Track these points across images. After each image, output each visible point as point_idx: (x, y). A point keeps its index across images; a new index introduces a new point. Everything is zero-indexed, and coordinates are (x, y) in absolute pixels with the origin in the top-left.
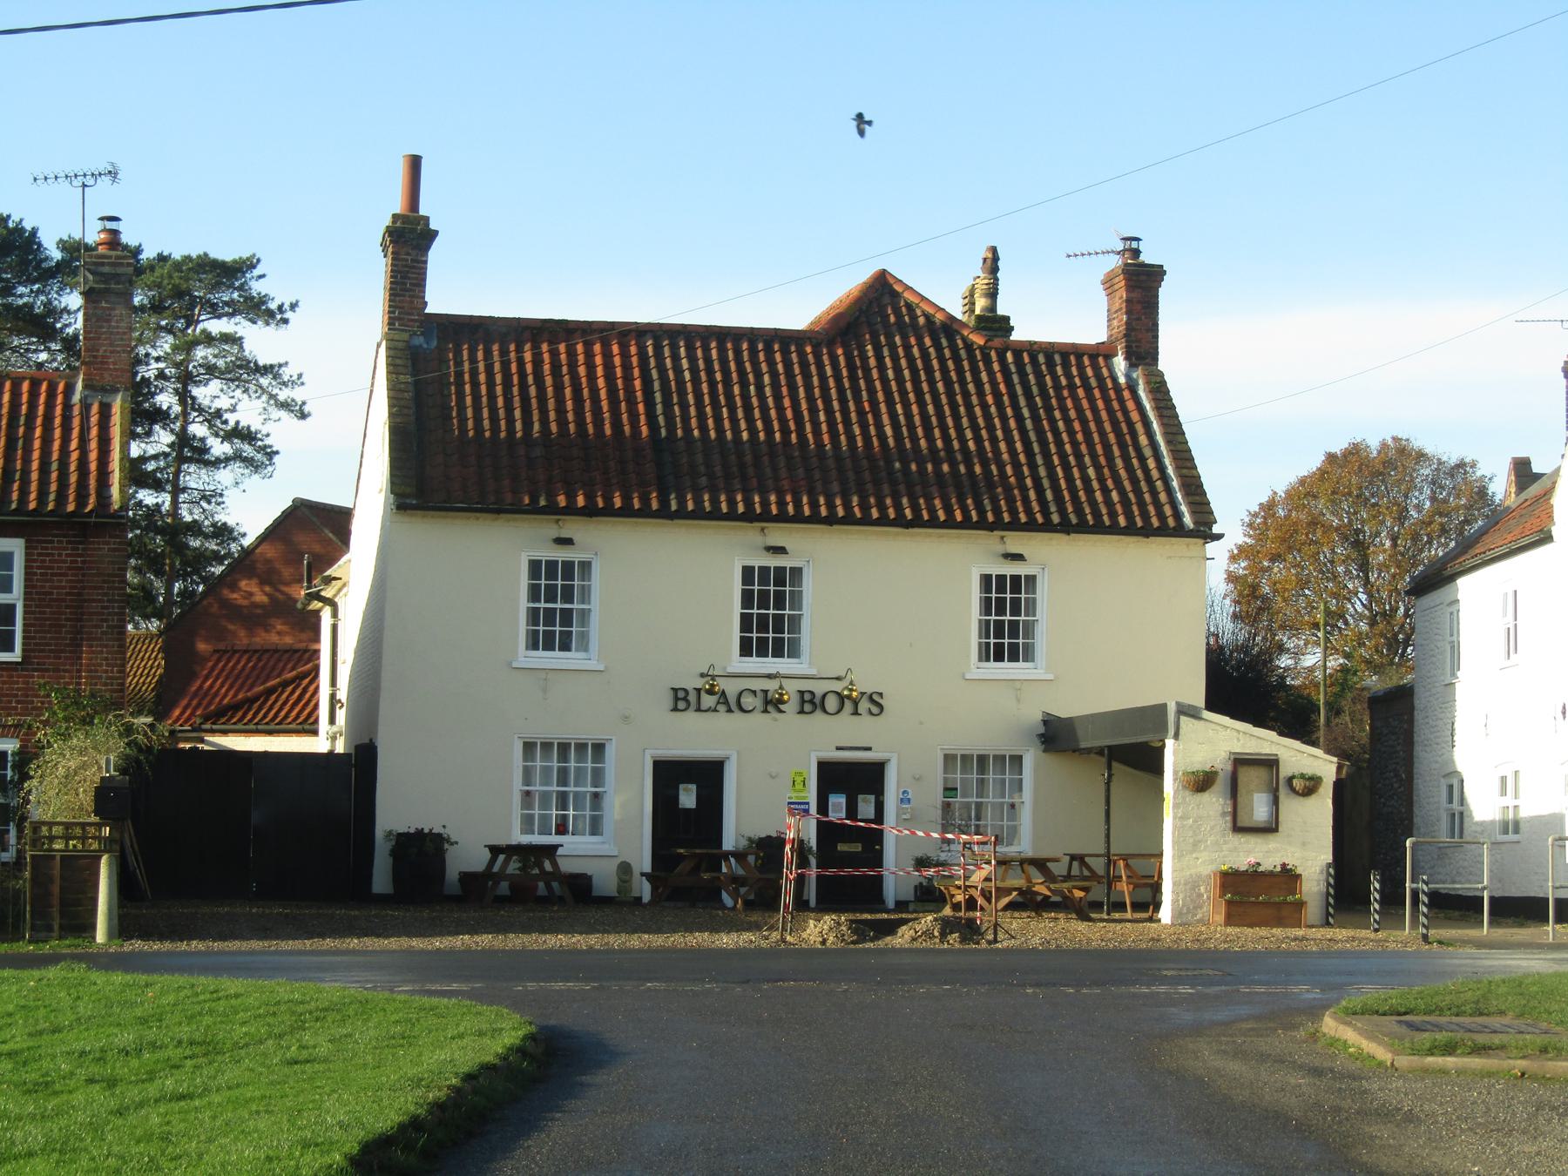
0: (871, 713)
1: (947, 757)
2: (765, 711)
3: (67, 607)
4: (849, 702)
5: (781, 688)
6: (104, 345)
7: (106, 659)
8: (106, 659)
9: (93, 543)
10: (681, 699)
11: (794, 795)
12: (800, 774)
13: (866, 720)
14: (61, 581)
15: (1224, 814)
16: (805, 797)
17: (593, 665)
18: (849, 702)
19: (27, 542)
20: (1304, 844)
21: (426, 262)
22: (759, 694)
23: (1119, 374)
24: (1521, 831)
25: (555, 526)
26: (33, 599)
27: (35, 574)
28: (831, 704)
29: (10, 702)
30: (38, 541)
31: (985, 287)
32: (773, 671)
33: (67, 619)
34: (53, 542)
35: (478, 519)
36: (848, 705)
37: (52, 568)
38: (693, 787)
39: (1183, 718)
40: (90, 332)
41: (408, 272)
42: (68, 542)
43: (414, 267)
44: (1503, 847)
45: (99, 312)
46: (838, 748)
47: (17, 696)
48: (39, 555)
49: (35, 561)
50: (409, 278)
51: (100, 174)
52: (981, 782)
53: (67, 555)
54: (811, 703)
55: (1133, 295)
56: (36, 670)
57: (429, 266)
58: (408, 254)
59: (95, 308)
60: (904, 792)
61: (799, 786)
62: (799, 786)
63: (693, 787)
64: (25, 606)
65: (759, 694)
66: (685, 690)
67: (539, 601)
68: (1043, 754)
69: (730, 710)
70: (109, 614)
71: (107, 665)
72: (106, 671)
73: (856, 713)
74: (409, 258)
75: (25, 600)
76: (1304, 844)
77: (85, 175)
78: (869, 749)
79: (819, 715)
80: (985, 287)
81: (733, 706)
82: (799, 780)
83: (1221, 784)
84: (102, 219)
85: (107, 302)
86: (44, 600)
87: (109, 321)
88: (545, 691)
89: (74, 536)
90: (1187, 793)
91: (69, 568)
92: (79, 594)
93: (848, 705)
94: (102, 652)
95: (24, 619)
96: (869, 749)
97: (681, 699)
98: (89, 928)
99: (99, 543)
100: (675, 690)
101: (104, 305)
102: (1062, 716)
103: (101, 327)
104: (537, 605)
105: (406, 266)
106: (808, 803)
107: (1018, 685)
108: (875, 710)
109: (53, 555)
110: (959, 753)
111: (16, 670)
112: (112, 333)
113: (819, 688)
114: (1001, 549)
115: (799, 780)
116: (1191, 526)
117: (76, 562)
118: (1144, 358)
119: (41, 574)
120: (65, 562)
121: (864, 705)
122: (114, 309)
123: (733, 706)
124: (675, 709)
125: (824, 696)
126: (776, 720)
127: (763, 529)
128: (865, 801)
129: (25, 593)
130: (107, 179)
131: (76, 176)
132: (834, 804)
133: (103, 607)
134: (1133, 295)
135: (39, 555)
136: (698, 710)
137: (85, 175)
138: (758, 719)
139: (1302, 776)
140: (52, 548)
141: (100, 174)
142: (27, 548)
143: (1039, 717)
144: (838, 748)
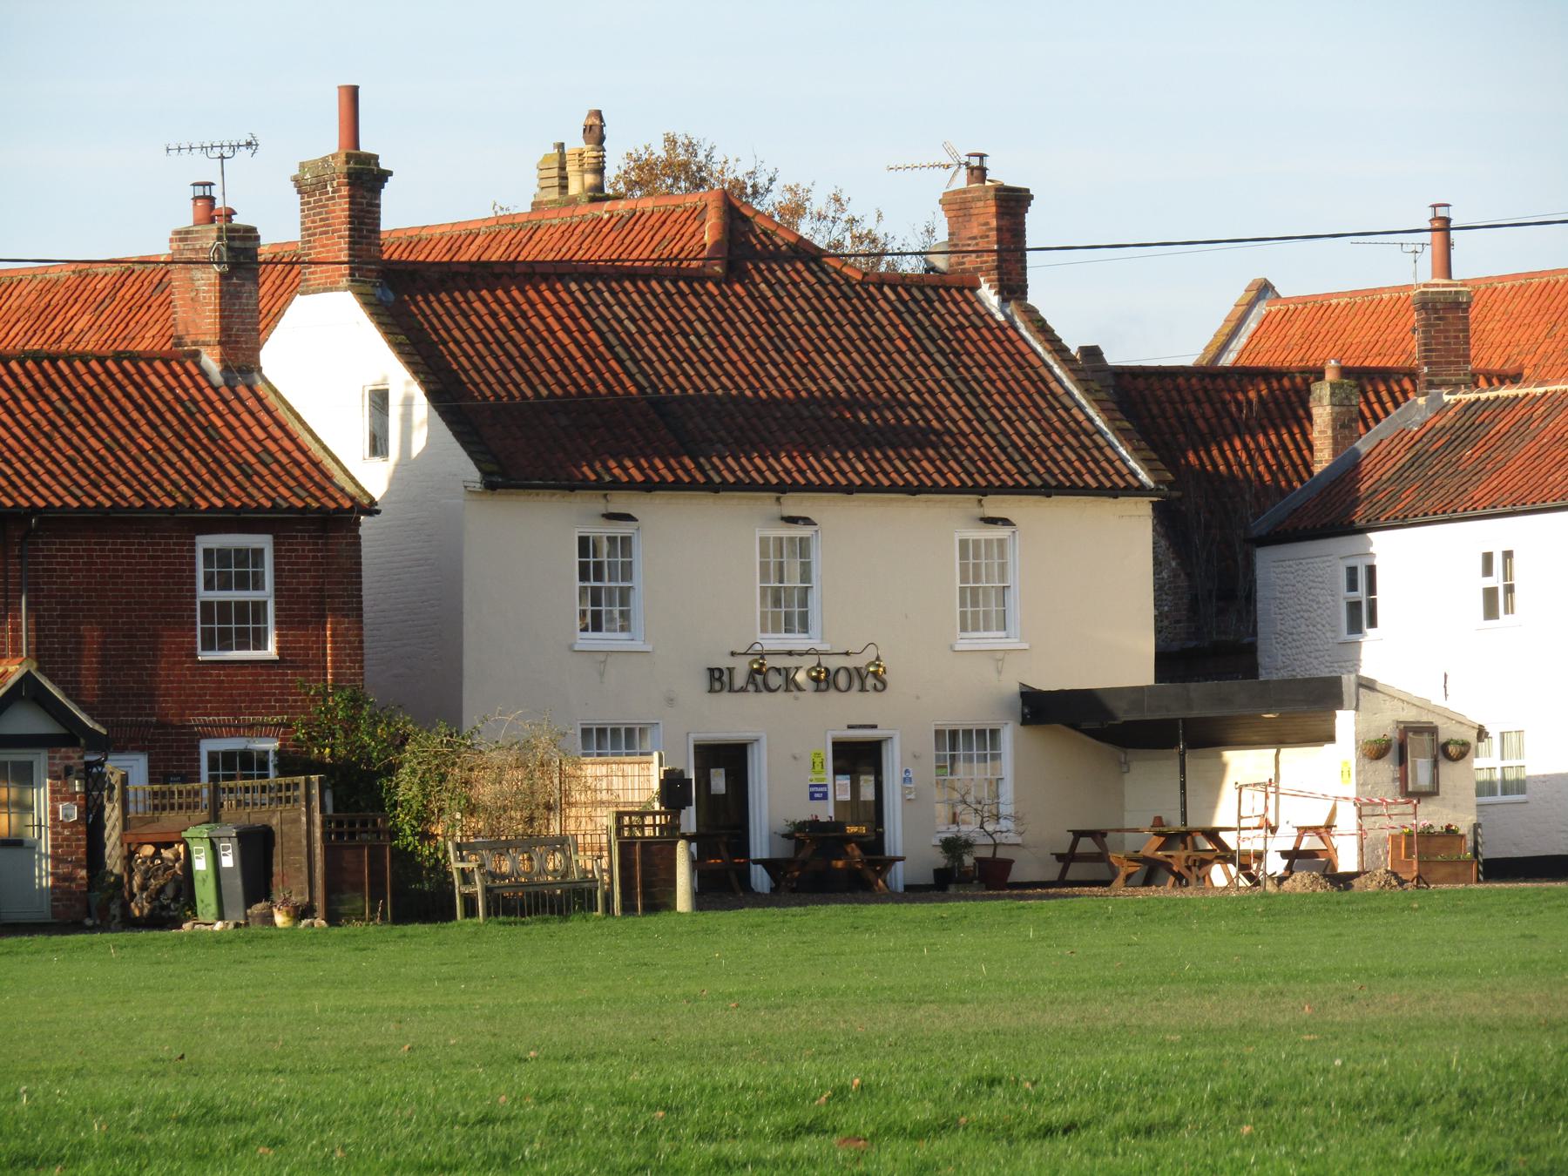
0: (875, 688)
1: (937, 732)
2: (787, 690)
3: (312, 603)
4: (858, 678)
5: (819, 665)
6: (236, 323)
7: (349, 655)
8: (349, 655)
9: (334, 537)
10: (718, 679)
11: (814, 777)
12: (818, 755)
13: (872, 696)
14: (305, 577)
15: (1394, 780)
16: (823, 779)
17: (638, 645)
18: (858, 678)
19: (275, 538)
20: (1455, 806)
21: (378, 206)
22: (783, 672)
23: (994, 310)
24: (1528, 791)
25: (604, 501)
26: (283, 597)
27: (284, 570)
28: (842, 680)
29: (270, 701)
30: (285, 537)
31: (594, 161)
32: (805, 648)
33: (312, 616)
34: (296, 537)
35: (538, 495)
36: (856, 684)
37: (297, 564)
38: (722, 771)
39: (1362, 690)
40: (225, 310)
41: (364, 217)
42: (310, 537)
43: (369, 212)
44: (1490, 809)
45: (232, 289)
46: (850, 727)
47: (274, 694)
48: (287, 550)
49: (283, 557)
50: (366, 224)
51: (239, 146)
52: (953, 758)
53: (309, 551)
54: (824, 681)
55: (1003, 222)
56: (289, 668)
57: (383, 209)
58: (364, 197)
59: (229, 285)
60: (907, 771)
61: (818, 768)
62: (818, 768)
63: (722, 771)
64: (276, 603)
65: (783, 672)
66: (720, 670)
67: (589, 580)
68: (1021, 729)
69: (757, 690)
70: (349, 610)
71: (351, 661)
72: (349, 668)
73: (863, 689)
74: (365, 201)
75: (276, 597)
76: (1455, 806)
77: (222, 146)
78: (875, 727)
79: (832, 694)
80: (594, 161)
81: (761, 686)
82: (818, 761)
83: (1393, 754)
84: (195, 185)
85: (238, 278)
86: (292, 596)
87: (239, 298)
88: (602, 675)
89: (315, 531)
90: (1367, 761)
91: (312, 564)
92: (322, 590)
93: (856, 684)
94: (345, 648)
95: (276, 616)
96: (875, 727)
97: (718, 679)
98: (670, 905)
99: (337, 538)
100: (711, 670)
101: (235, 280)
102: (1045, 688)
103: (234, 305)
104: (586, 584)
105: (362, 211)
106: (826, 786)
107: (999, 655)
108: (879, 686)
109: (297, 550)
110: (961, 728)
111: (273, 668)
112: (243, 310)
113: (833, 663)
114: (979, 512)
115: (818, 761)
116: (1152, 485)
117: (317, 557)
118: (1015, 292)
119: (289, 570)
120: (307, 557)
121: (870, 681)
122: (243, 285)
123: (854, 674)
124: (711, 690)
125: (837, 671)
126: (796, 698)
127: (778, 499)
128: (866, 781)
129: (276, 590)
130: (244, 152)
131: (212, 147)
132: (846, 791)
133: (344, 603)
134: (1003, 222)
135: (287, 550)
136: (731, 690)
137: (222, 146)
138: (810, 697)
139: (1456, 742)
140: (297, 544)
141: (239, 146)
142: (275, 544)
143: (1016, 689)
144: (850, 727)
